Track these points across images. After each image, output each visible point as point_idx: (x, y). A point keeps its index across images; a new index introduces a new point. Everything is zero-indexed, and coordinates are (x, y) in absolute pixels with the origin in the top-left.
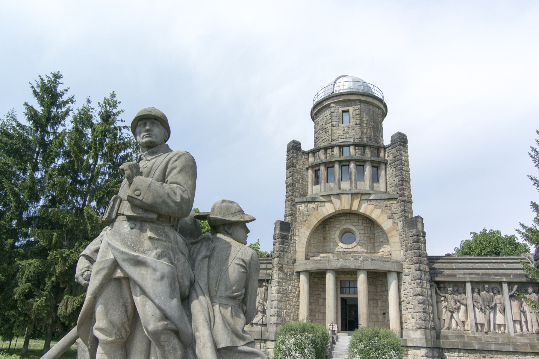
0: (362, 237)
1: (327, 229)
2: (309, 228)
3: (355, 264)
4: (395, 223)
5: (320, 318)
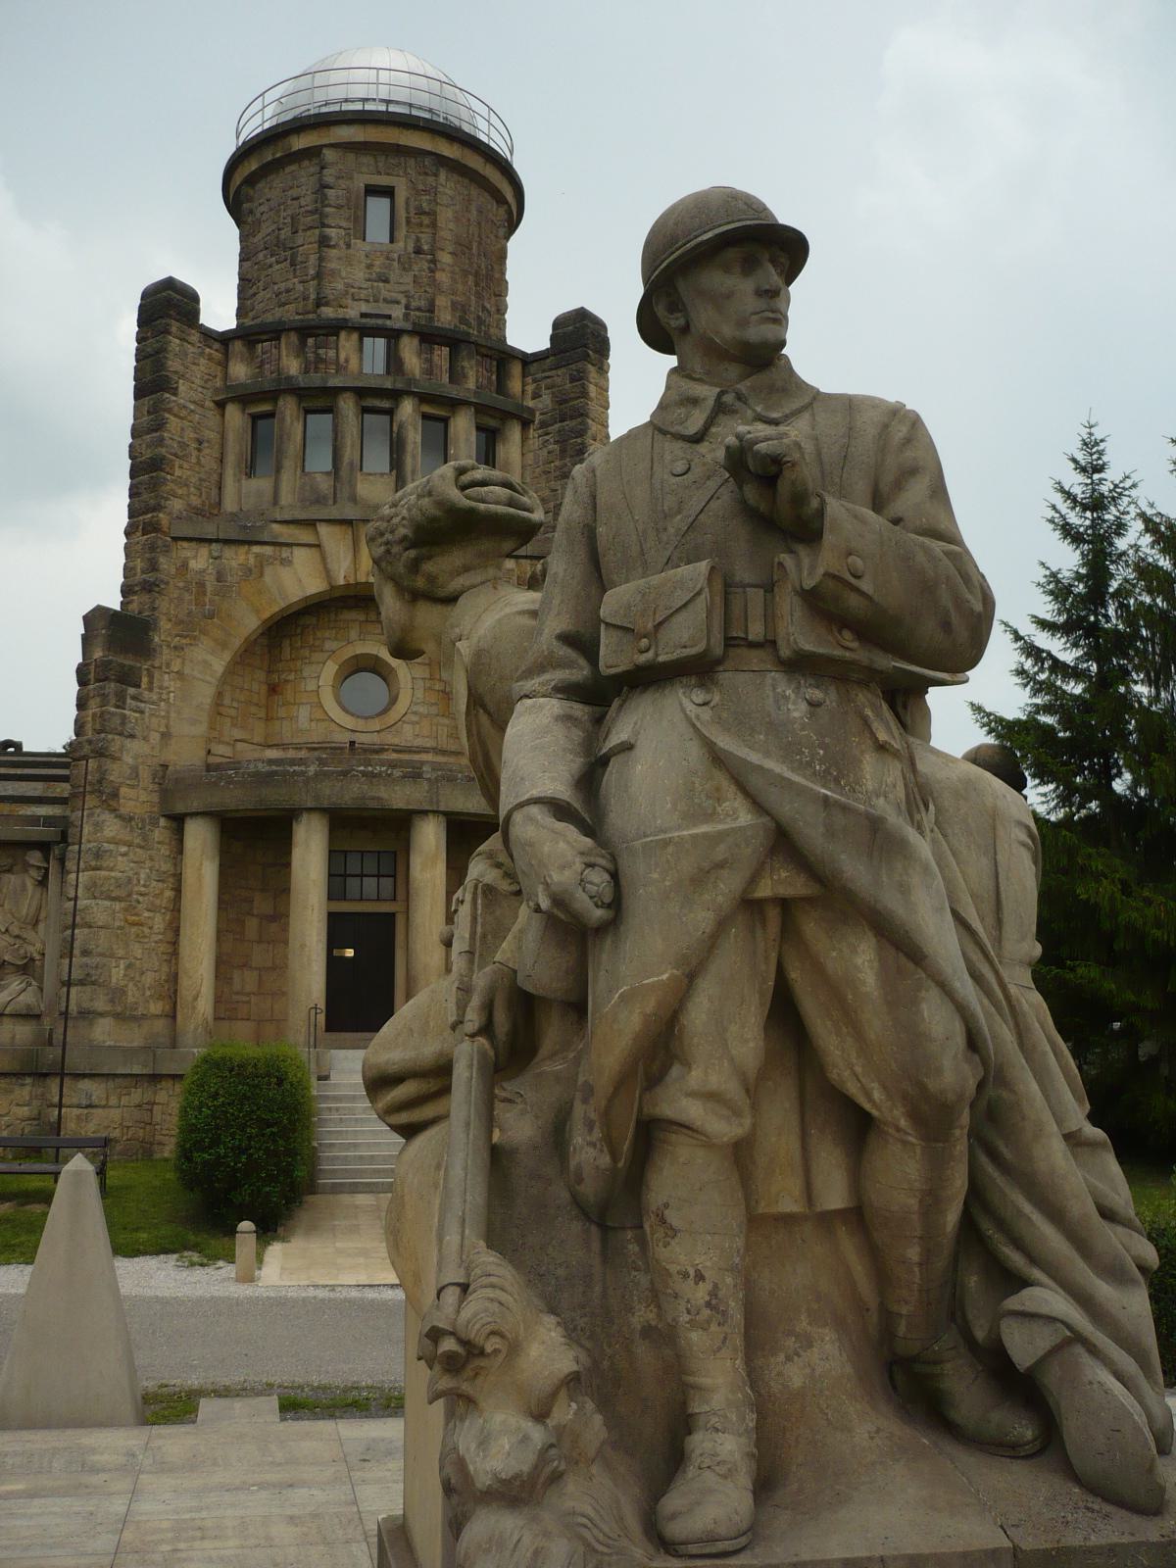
0: (419, 694)
1: (287, 652)
2: (224, 645)
5: (248, 988)
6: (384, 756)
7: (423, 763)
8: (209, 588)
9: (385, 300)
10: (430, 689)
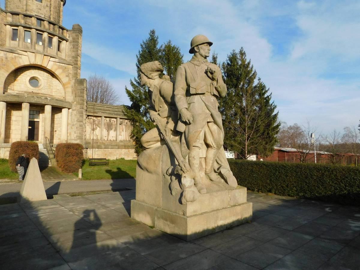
2: (7, 71)
3: (45, 101)
4: (70, 80)
6: (39, 95)
7: (47, 96)
8: (4, 60)
9: (40, 14)
10: (47, 84)
